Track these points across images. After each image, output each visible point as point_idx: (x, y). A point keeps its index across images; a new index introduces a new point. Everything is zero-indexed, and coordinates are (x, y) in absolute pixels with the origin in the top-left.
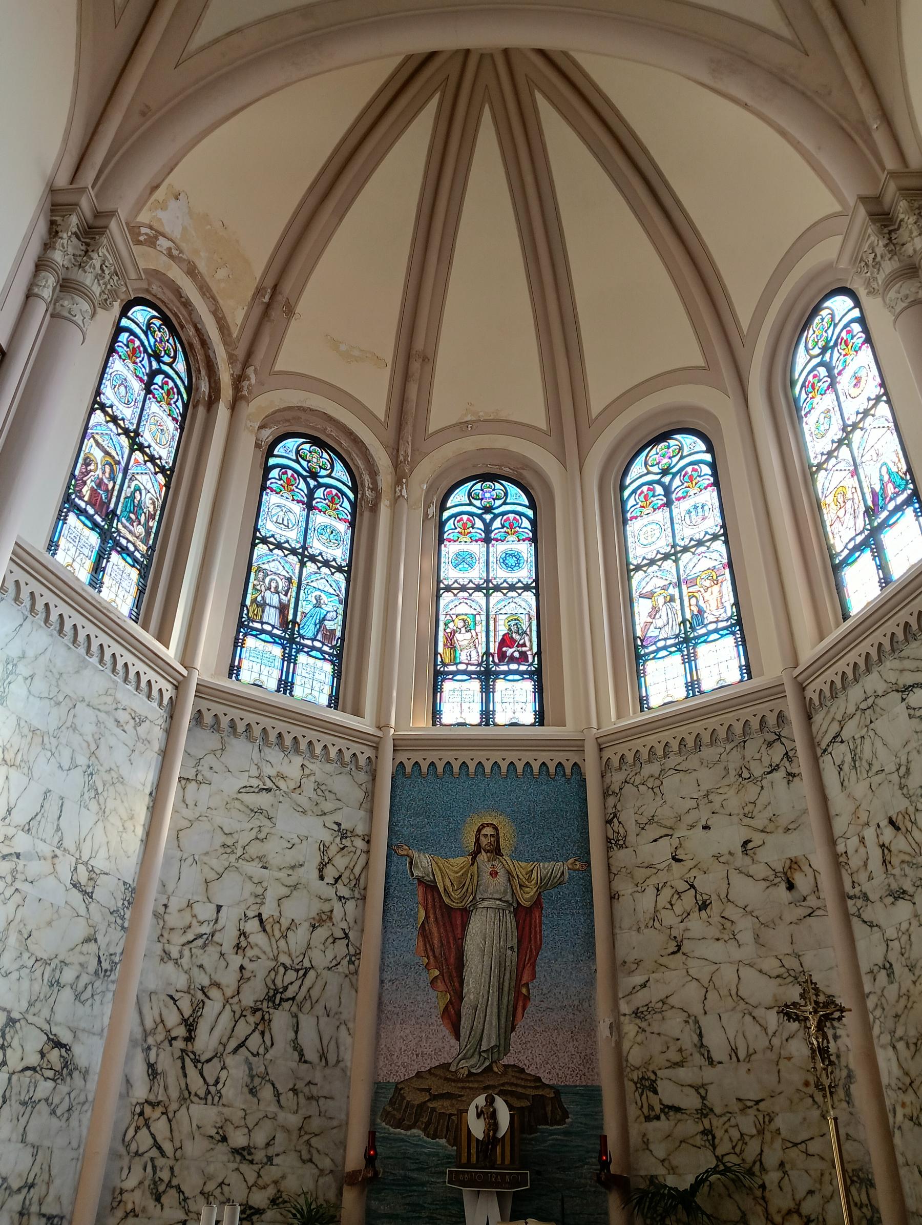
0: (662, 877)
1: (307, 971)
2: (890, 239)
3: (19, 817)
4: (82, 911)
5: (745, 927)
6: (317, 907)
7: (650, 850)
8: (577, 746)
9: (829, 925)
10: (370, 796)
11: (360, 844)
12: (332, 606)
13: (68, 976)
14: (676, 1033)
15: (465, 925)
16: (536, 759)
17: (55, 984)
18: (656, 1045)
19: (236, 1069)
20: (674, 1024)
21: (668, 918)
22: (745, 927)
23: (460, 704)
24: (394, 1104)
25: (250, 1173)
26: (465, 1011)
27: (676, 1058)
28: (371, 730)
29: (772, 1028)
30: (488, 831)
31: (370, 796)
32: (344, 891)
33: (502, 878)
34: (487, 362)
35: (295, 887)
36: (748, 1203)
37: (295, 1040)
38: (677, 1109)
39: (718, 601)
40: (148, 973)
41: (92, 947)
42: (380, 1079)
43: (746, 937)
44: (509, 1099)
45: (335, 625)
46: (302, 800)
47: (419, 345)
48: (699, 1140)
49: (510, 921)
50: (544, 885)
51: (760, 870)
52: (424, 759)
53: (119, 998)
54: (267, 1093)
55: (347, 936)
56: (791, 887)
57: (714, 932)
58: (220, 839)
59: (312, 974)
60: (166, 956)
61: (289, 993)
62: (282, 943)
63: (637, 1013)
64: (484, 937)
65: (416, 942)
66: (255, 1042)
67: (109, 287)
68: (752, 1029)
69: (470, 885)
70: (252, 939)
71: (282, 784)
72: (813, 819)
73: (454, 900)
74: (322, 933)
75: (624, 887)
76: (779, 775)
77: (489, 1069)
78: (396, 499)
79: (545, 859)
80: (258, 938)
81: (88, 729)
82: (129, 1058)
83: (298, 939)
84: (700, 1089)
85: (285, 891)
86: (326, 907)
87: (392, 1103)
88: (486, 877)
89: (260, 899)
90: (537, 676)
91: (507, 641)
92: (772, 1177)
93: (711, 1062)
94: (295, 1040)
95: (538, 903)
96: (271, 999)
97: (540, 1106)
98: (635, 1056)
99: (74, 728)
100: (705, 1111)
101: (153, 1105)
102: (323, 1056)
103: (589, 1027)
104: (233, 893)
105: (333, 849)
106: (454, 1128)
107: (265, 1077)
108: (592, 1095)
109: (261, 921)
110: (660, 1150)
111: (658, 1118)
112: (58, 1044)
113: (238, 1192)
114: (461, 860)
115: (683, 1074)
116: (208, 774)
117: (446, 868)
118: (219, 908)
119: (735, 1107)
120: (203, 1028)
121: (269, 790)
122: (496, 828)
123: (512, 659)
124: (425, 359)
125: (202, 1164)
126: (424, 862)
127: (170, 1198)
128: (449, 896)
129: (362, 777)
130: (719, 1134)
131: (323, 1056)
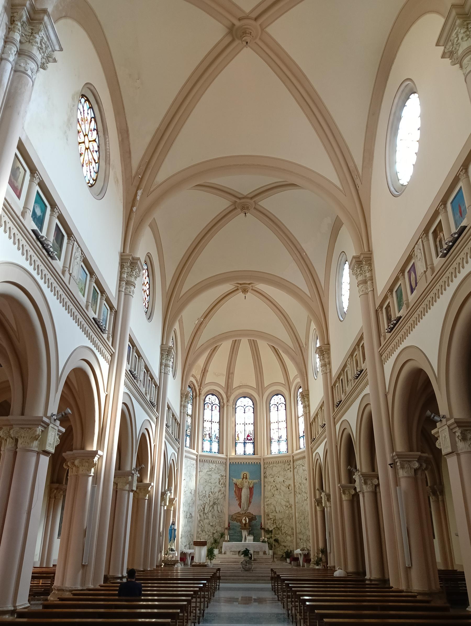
0: (272, 484)
2: (467, 28)
5: (282, 494)
6: (219, 489)
7: (270, 479)
8: (260, 459)
10: (226, 469)
11: (224, 477)
12: (217, 432)
15: (241, 491)
16: (253, 461)
20: (272, 507)
21: (272, 491)
22: (282, 494)
23: (240, 449)
24: (232, 518)
25: (213, 528)
28: (225, 457)
31: (226, 469)
32: (223, 486)
34: (244, 373)
36: (280, 532)
39: (284, 437)
40: (199, 502)
43: (282, 495)
44: (349, 120)
45: (218, 435)
47: (231, 372)
49: (249, 490)
50: (254, 484)
51: (285, 485)
53: (195, 506)
54: (214, 517)
57: (278, 494)
58: (205, 480)
60: (200, 499)
63: (267, 505)
64: (245, 493)
65: (234, 493)
66: (212, 510)
67: (46, 55)
68: (282, 509)
69: (242, 484)
72: (292, 479)
73: (240, 486)
74: (220, 493)
75: (266, 485)
76: (289, 470)
78: (227, 405)
80: (211, 495)
83: (217, 494)
84: (275, 516)
89: (211, 489)
90: (253, 443)
91: (248, 436)
92: (283, 529)
97: (252, 518)
98: (266, 511)
103: (260, 507)
104: (207, 489)
106: (241, 522)
107: (214, 515)
108: (260, 517)
110: (269, 524)
113: (212, 531)
115: (273, 514)
120: (205, 509)
123: (249, 440)
124: (232, 373)
125: (207, 528)
127: (204, 532)
129: (224, 465)
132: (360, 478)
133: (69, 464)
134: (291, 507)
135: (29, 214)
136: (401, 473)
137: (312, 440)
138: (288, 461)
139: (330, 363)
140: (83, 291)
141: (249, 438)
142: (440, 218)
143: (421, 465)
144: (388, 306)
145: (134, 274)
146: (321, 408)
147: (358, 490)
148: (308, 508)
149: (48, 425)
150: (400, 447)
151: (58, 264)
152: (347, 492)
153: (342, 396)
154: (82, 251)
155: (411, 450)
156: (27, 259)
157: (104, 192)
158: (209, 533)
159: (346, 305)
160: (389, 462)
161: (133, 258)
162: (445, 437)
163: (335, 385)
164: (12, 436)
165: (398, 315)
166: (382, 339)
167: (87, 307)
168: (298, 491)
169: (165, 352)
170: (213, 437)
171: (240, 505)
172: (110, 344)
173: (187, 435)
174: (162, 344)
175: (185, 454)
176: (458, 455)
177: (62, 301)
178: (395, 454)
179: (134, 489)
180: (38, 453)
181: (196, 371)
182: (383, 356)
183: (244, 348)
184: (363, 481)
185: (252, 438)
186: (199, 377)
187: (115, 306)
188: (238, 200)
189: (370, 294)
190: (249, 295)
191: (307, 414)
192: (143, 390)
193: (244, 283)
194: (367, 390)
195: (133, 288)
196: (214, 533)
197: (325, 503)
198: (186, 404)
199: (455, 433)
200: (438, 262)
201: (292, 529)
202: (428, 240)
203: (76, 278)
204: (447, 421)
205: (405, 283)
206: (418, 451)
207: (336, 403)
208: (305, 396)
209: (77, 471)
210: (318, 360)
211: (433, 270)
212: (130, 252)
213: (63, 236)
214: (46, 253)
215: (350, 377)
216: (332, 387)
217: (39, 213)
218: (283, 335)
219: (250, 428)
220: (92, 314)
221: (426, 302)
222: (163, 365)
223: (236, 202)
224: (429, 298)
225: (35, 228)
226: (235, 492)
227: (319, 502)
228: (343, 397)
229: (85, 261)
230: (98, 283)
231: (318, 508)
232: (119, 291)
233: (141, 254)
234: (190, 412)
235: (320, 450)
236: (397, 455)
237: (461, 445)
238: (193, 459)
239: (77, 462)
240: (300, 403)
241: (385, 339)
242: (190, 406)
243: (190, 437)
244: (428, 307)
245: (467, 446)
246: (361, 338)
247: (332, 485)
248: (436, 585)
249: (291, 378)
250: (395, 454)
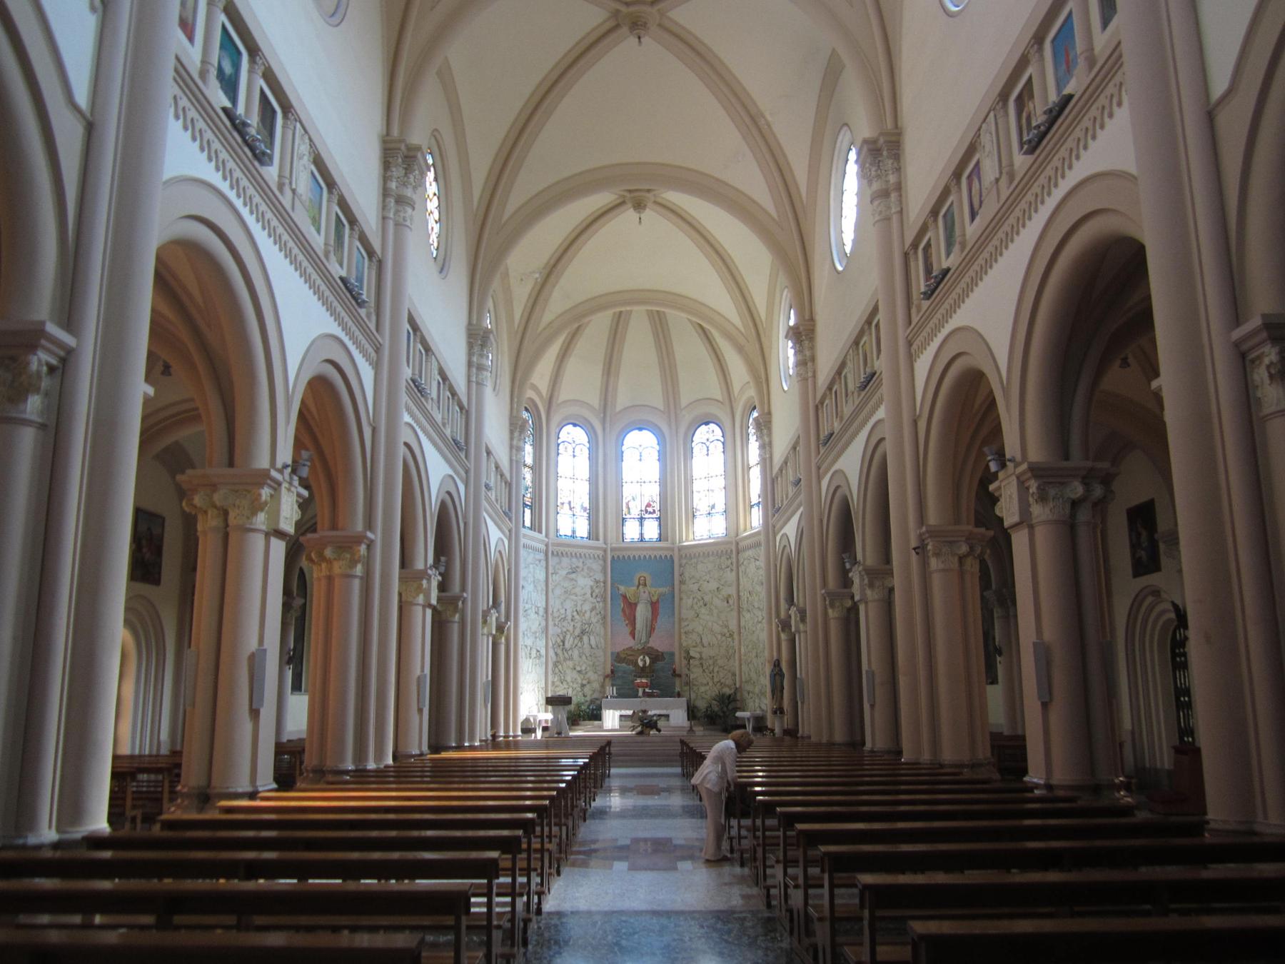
5: (715, 611)
8: (672, 549)
9: (735, 614)
16: (658, 553)
19: (576, 653)
24: (618, 658)
39: (720, 507)
45: (587, 505)
50: (660, 595)
52: (621, 554)
64: (642, 612)
73: (632, 601)
75: (684, 597)
91: (649, 505)
97: (656, 657)
104: (568, 605)
106: (636, 664)
108: (672, 654)
117: (630, 591)
126: (622, 589)
132: (861, 576)
133: (313, 555)
134: (731, 635)
135: (213, 73)
136: (934, 563)
137: (774, 507)
138: (730, 551)
139: (813, 359)
140: (316, 222)
141: (650, 509)
142: (1030, 70)
143: (972, 548)
144: (928, 245)
145: (412, 180)
146: (794, 448)
147: (857, 598)
148: (764, 636)
149: (279, 484)
150: (933, 517)
151: (271, 173)
152: (837, 604)
153: (836, 424)
154: (310, 140)
155: (957, 521)
156: (217, 169)
157: (342, 10)
159: (848, 236)
160: (914, 543)
161: (409, 148)
162: (1010, 497)
163: (822, 402)
164: (218, 504)
165: (945, 266)
166: (914, 310)
167: (327, 255)
168: (745, 606)
169: (477, 339)
170: (578, 511)
171: (633, 634)
172: (372, 326)
173: (525, 505)
174: (470, 323)
175: (523, 541)
176: (1031, 527)
177: (283, 247)
178: (924, 529)
179: (434, 602)
180: (267, 535)
181: (541, 376)
182: (915, 346)
183: (639, 337)
184: (866, 581)
185: (657, 507)
186: (544, 391)
187: (379, 252)
188: (624, 9)
189: (895, 218)
190: (648, 214)
191: (766, 461)
192: (438, 418)
193: (637, 189)
194: (881, 413)
195: (409, 210)
196: (583, 686)
197: (797, 627)
198: (521, 444)
199: (1028, 488)
200: (1021, 161)
201: (734, 675)
202: (1007, 114)
203: (304, 198)
204: (1015, 467)
205: (960, 201)
206: (968, 524)
207: (822, 440)
208: (764, 426)
209: (330, 569)
210: (791, 352)
211: (1011, 176)
212: (402, 132)
213: (274, 112)
214: (249, 154)
215: (851, 387)
216: (818, 404)
217: (228, 69)
218: (721, 301)
219: (652, 492)
220: (338, 271)
221: (995, 242)
222: (474, 367)
223: (618, 11)
224: (1001, 234)
225: (228, 104)
226: (623, 610)
227: (785, 625)
228: (837, 426)
229: (318, 162)
230: (343, 204)
231: (783, 636)
232: (384, 218)
233: (418, 136)
234: (529, 460)
235: (791, 529)
236: (927, 531)
237: (1037, 510)
238: (536, 550)
239: (328, 552)
240: (753, 438)
241: (919, 311)
242: (528, 449)
243: (531, 508)
244: (998, 252)
245: (1047, 510)
246: (875, 310)
247: (809, 592)
248: (984, 752)
249: (736, 387)
250: (924, 529)
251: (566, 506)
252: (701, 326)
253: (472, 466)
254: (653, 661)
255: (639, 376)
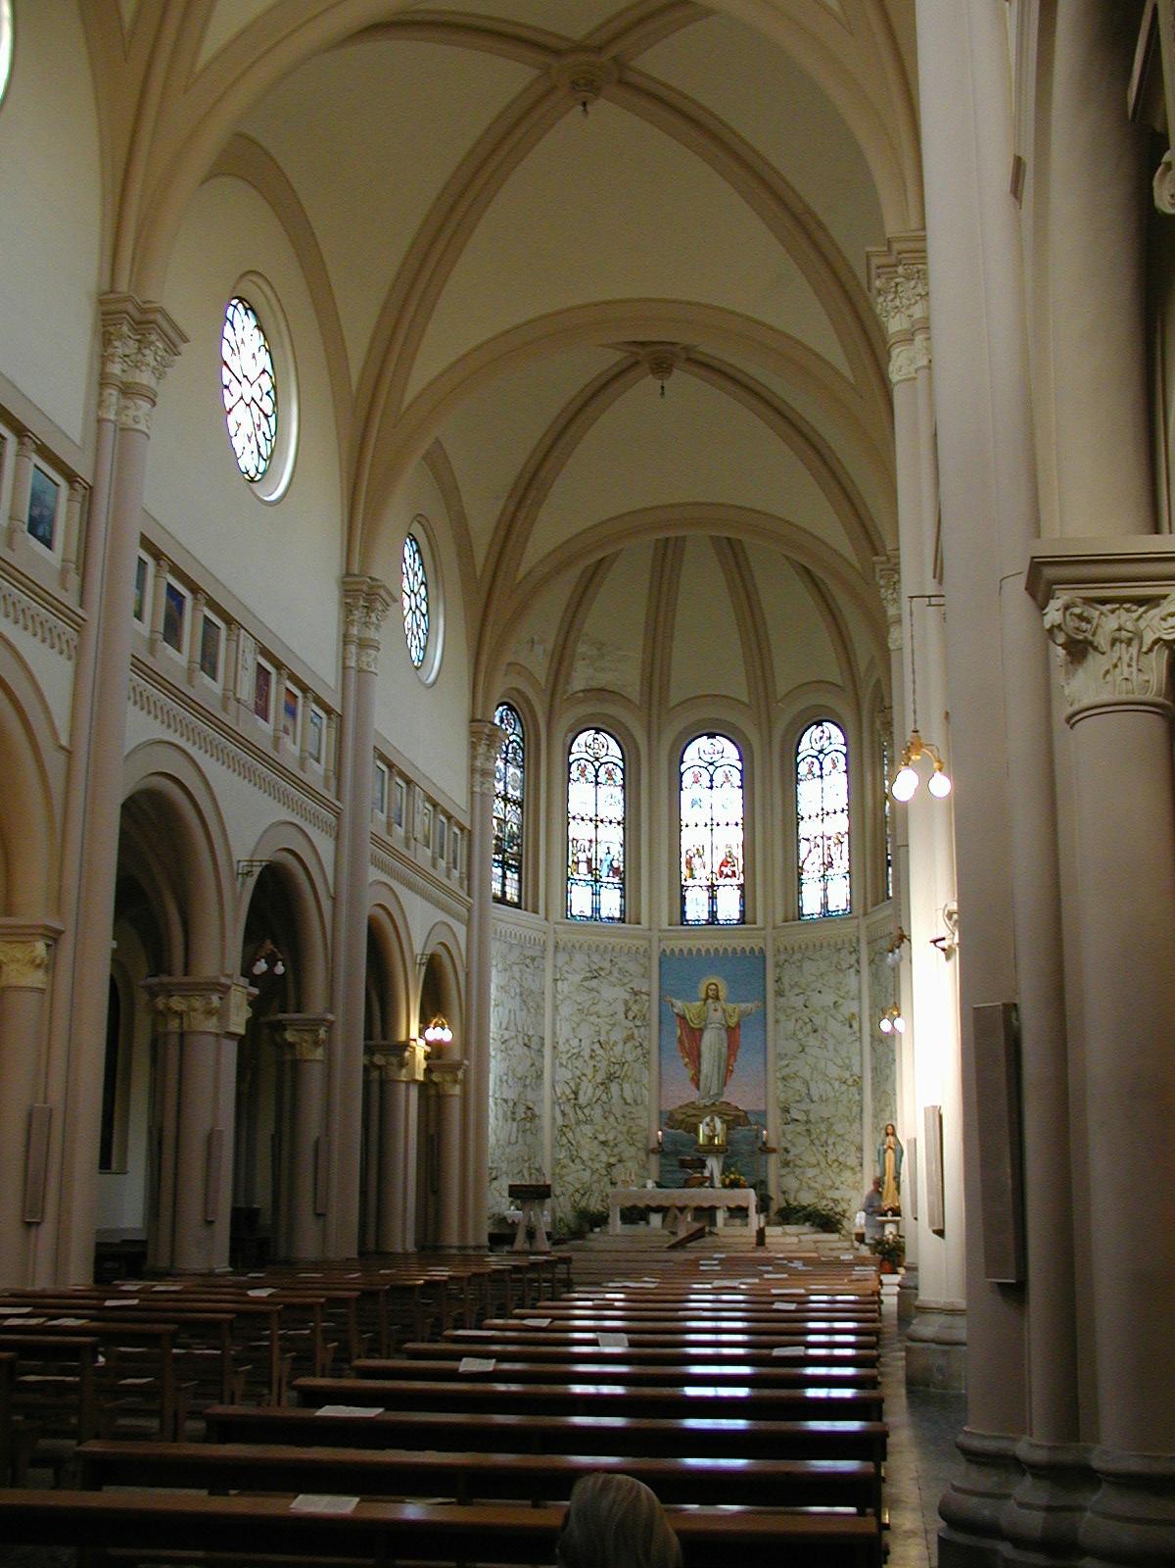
1: (624, 1064)
3: (504, 1026)
4: (528, 1053)
5: (831, 1042)
6: (625, 1034)
12: (617, 850)
13: (528, 1082)
14: (798, 1088)
15: (701, 1036)
17: (525, 1086)
18: (791, 1093)
19: (598, 1112)
20: (798, 1085)
21: (800, 1035)
26: (702, 1078)
27: (798, 1098)
29: (837, 1087)
30: (713, 987)
32: (639, 1023)
33: (719, 1014)
35: (614, 1025)
37: (622, 1095)
38: (797, 1120)
41: (534, 1068)
42: (662, 1109)
43: (831, 1048)
46: (613, 979)
48: (804, 1133)
49: (724, 1035)
50: (743, 1014)
54: (612, 1119)
55: (641, 1045)
56: (851, 1026)
58: (576, 1007)
59: (626, 1065)
61: (616, 1075)
62: (611, 1053)
65: (676, 1045)
70: (598, 1052)
71: (602, 974)
74: (629, 1045)
76: (852, 970)
77: (713, 1104)
79: (743, 1001)
80: (600, 1052)
81: (517, 975)
82: (553, 1109)
85: (609, 1027)
86: (630, 1032)
87: (669, 1119)
88: (711, 1012)
89: (598, 1033)
91: (724, 864)
93: (812, 1101)
94: (622, 1095)
95: (738, 1025)
96: (608, 1078)
97: (736, 1121)
99: (514, 978)
100: (808, 1122)
101: (566, 1126)
102: (635, 1101)
104: (586, 1032)
105: (631, 1002)
107: (610, 1112)
109: (601, 1044)
111: (789, 1124)
112: (530, 1109)
113: (604, 1158)
114: (698, 1003)
116: (566, 975)
118: (580, 1040)
119: (819, 1120)
120: (581, 1093)
121: (595, 977)
122: (716, 985)
123: (727, 876)
127: (577, 1161)
128: (692, 1022)
130: (812, 1131)
131: (635, 1101)
141: (727, 870)
158: (597, 1166)
171: (696, 1081)
183: (703, 588)
185: (739, 869)
251: (583, 868)
252: (807, 571)
253: (346, 806)
254: (730, 1126)
255: (707, 649)
